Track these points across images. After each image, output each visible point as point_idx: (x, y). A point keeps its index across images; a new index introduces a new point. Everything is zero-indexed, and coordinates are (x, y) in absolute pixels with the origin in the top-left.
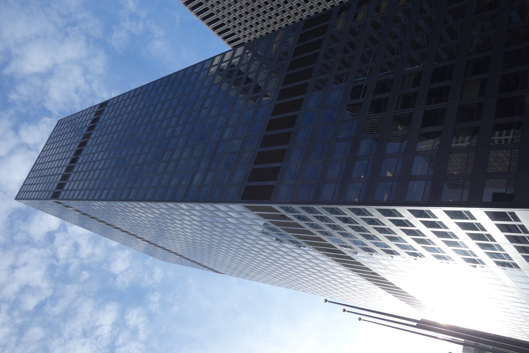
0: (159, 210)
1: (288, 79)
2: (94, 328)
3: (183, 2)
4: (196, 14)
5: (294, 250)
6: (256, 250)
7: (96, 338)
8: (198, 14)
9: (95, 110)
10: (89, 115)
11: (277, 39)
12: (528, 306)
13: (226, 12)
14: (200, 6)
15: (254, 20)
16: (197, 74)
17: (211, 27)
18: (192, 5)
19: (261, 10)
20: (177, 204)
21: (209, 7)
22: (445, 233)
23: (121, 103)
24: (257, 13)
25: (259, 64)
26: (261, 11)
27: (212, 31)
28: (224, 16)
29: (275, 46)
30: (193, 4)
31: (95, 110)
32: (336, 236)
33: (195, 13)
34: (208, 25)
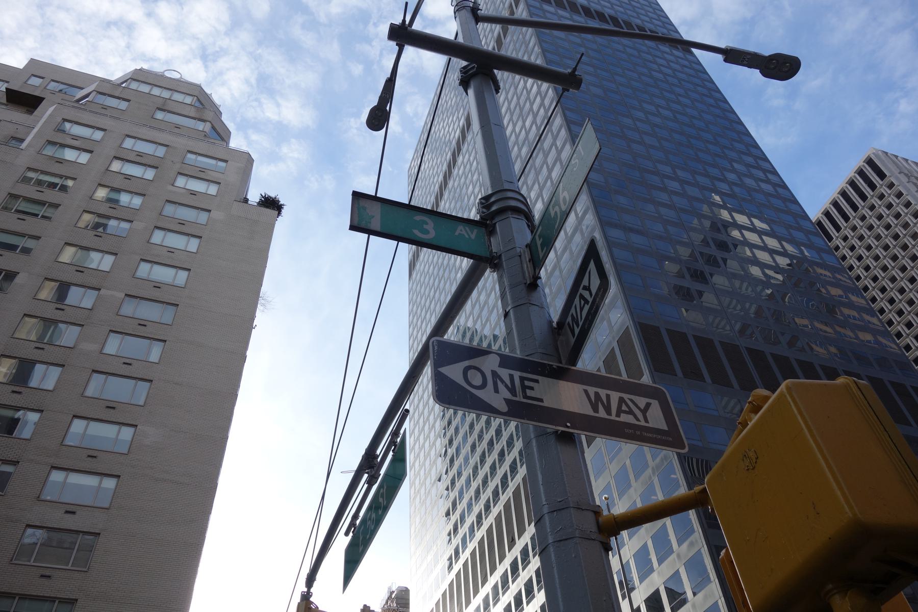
0: (463, 174)
1: (732, 350)
2: (271, 93)
3: (872, 155)
4: (826, 211)
5: (417, 396)
6: (441, 297)
7: (257, 100)
8: (835, 204)
9: (645, 23)
10: (635, 14)
11: (817, 324)
12: (913, 189)
13: (864, 231)
14: (850, 207)
15: (913, 220)
16: (739, 182)
17: (847, 187)
18: (869, 171)
19: (896, 273)
20: (554, 101)
21: (877, 192)
22: (498, 594)
23: (671, 55)
24: (869, 287)
25: (726, 332)
26: (874, 292)
27: (831, 200)
28: (854, 228)
29: (805, 322)
30: (870, 173)
31: (645, 23)
32: (478, 425)
33: (853, 178)
34: (842, 192)
